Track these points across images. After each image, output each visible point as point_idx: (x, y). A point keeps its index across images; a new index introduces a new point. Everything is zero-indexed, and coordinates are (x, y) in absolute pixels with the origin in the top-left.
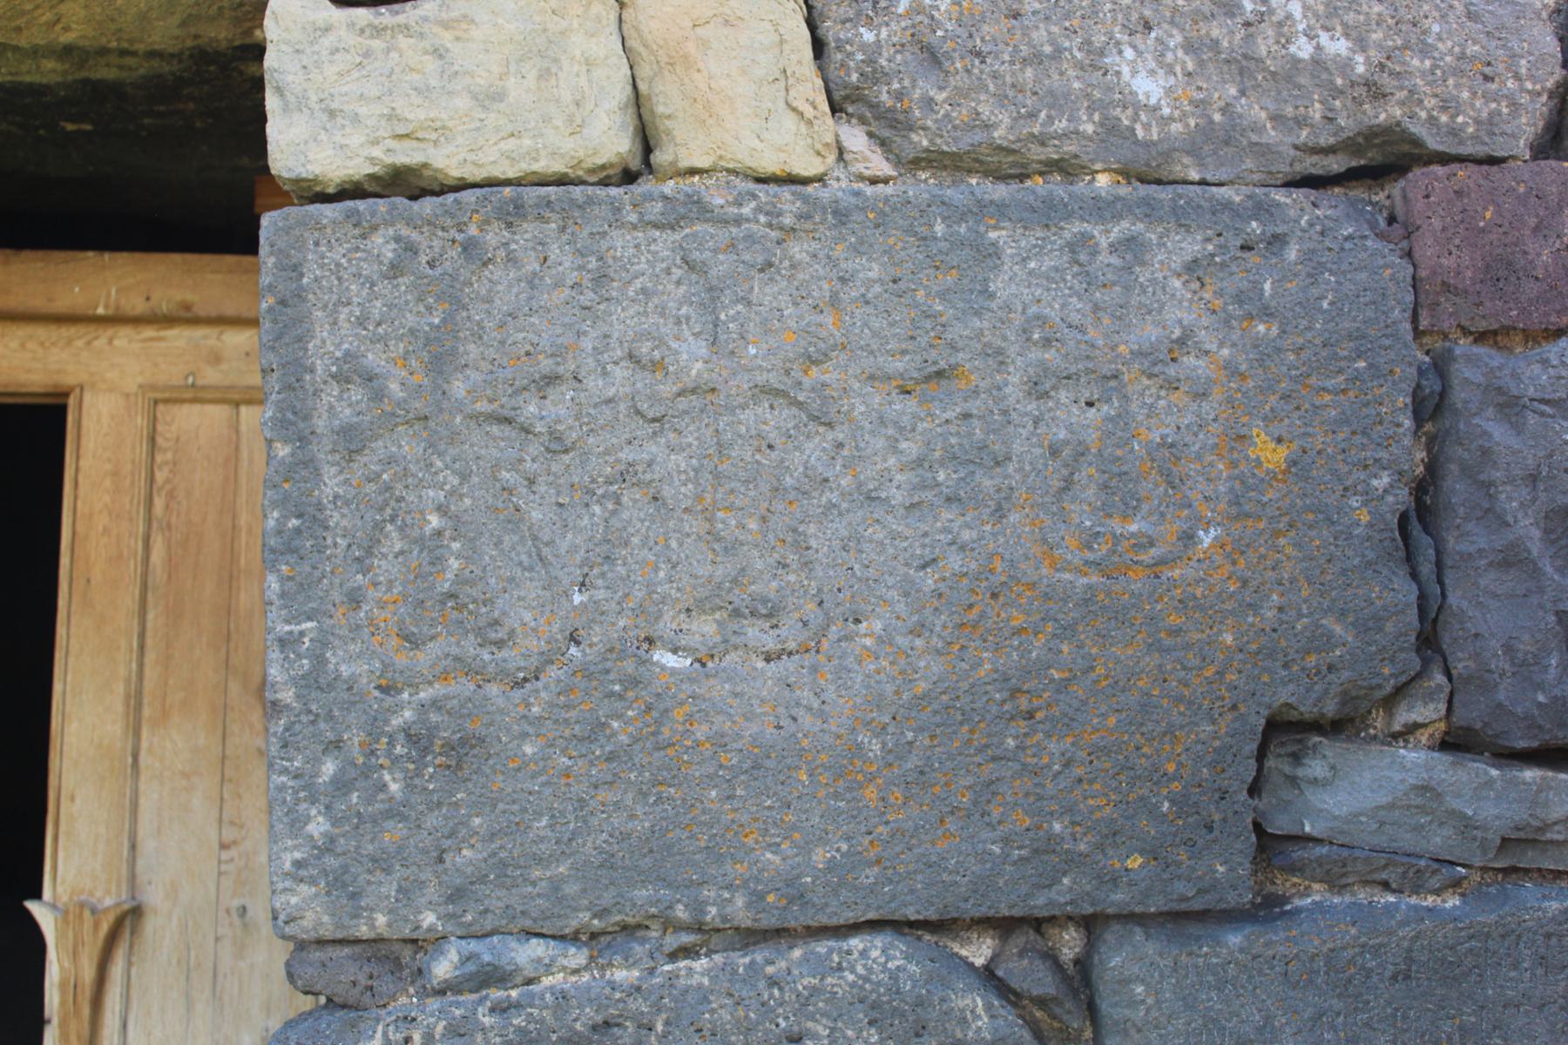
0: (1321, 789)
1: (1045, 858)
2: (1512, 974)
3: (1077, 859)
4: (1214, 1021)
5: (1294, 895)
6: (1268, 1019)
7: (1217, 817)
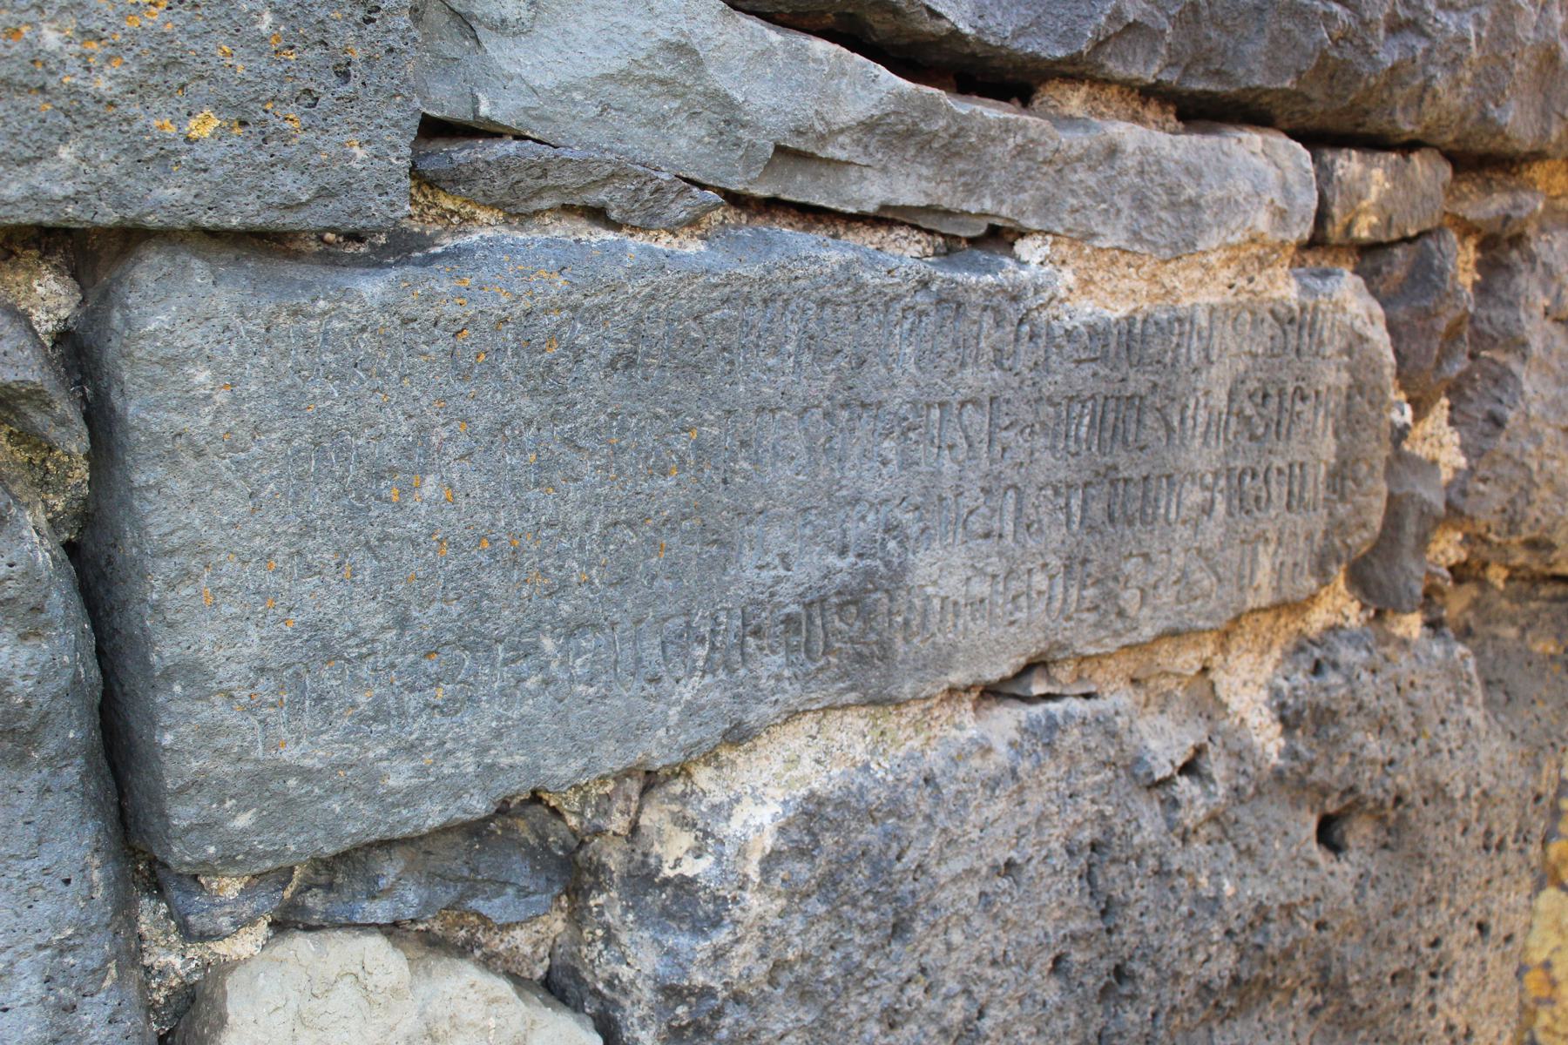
0: (510, 42)
1: (24, 101)
2: (771, 362)
3: (91, 108)
4: (336, 434)
5: (439, 233)
6: (423, 430)
7: (358, 55)
